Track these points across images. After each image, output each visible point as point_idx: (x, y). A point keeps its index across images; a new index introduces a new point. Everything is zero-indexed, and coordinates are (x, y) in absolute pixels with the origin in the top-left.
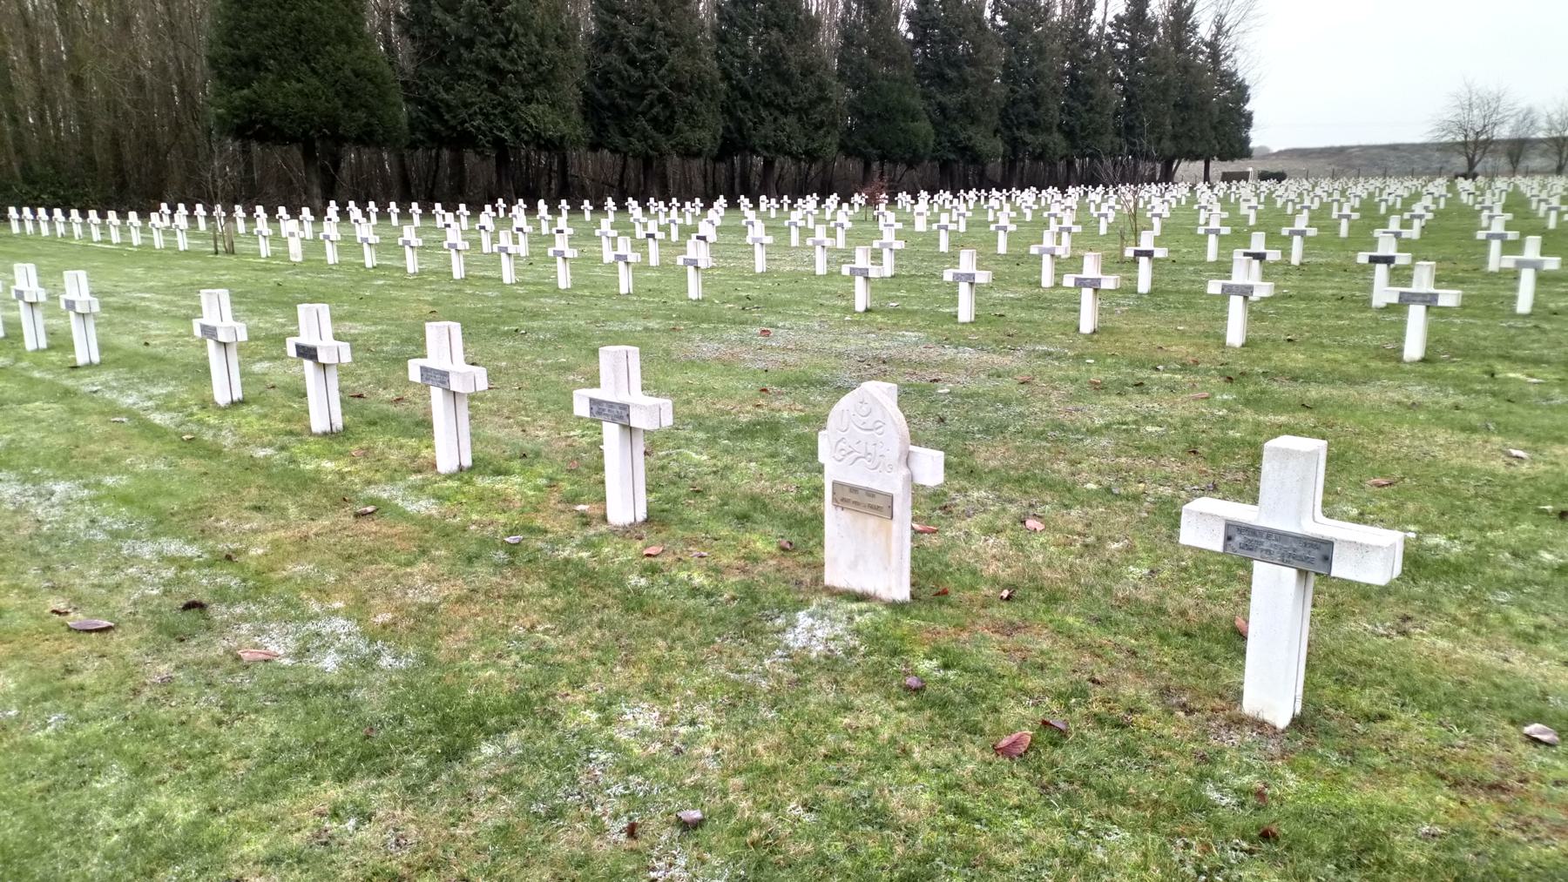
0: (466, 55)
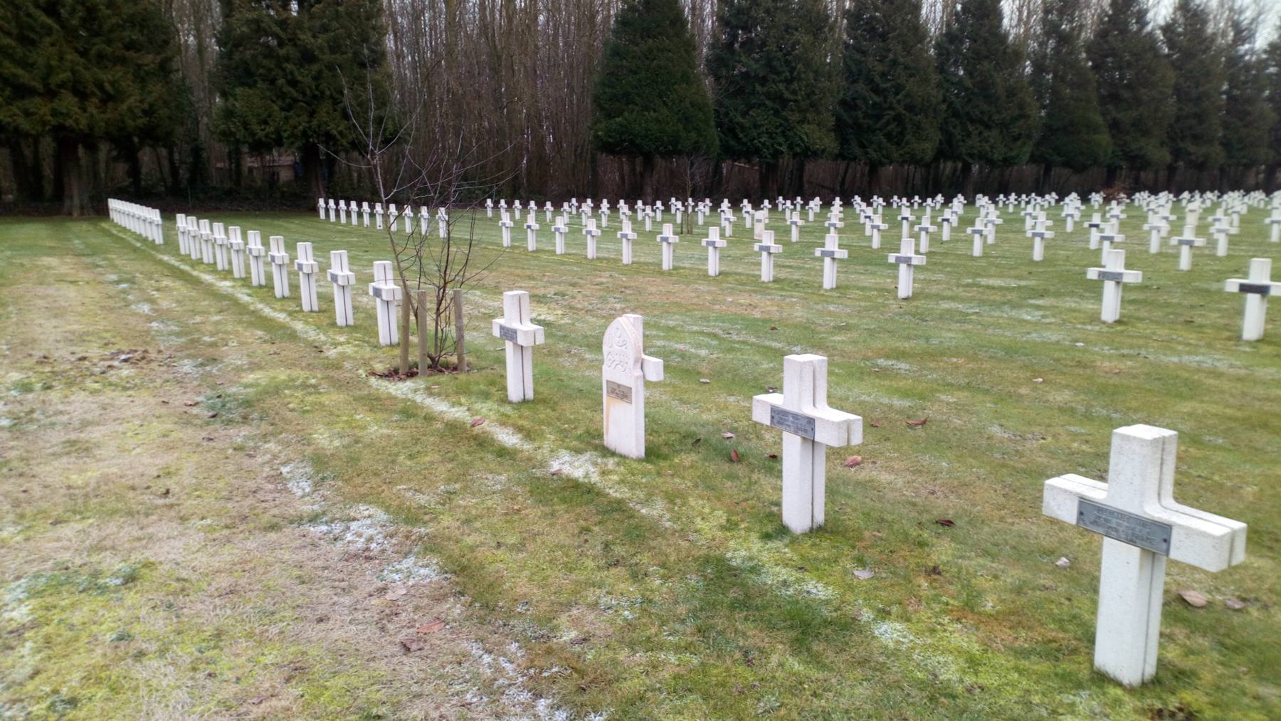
0: (758, 88)
